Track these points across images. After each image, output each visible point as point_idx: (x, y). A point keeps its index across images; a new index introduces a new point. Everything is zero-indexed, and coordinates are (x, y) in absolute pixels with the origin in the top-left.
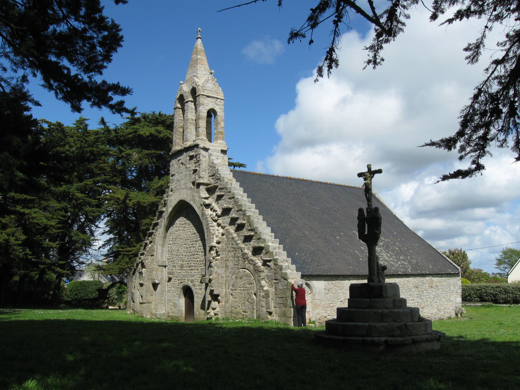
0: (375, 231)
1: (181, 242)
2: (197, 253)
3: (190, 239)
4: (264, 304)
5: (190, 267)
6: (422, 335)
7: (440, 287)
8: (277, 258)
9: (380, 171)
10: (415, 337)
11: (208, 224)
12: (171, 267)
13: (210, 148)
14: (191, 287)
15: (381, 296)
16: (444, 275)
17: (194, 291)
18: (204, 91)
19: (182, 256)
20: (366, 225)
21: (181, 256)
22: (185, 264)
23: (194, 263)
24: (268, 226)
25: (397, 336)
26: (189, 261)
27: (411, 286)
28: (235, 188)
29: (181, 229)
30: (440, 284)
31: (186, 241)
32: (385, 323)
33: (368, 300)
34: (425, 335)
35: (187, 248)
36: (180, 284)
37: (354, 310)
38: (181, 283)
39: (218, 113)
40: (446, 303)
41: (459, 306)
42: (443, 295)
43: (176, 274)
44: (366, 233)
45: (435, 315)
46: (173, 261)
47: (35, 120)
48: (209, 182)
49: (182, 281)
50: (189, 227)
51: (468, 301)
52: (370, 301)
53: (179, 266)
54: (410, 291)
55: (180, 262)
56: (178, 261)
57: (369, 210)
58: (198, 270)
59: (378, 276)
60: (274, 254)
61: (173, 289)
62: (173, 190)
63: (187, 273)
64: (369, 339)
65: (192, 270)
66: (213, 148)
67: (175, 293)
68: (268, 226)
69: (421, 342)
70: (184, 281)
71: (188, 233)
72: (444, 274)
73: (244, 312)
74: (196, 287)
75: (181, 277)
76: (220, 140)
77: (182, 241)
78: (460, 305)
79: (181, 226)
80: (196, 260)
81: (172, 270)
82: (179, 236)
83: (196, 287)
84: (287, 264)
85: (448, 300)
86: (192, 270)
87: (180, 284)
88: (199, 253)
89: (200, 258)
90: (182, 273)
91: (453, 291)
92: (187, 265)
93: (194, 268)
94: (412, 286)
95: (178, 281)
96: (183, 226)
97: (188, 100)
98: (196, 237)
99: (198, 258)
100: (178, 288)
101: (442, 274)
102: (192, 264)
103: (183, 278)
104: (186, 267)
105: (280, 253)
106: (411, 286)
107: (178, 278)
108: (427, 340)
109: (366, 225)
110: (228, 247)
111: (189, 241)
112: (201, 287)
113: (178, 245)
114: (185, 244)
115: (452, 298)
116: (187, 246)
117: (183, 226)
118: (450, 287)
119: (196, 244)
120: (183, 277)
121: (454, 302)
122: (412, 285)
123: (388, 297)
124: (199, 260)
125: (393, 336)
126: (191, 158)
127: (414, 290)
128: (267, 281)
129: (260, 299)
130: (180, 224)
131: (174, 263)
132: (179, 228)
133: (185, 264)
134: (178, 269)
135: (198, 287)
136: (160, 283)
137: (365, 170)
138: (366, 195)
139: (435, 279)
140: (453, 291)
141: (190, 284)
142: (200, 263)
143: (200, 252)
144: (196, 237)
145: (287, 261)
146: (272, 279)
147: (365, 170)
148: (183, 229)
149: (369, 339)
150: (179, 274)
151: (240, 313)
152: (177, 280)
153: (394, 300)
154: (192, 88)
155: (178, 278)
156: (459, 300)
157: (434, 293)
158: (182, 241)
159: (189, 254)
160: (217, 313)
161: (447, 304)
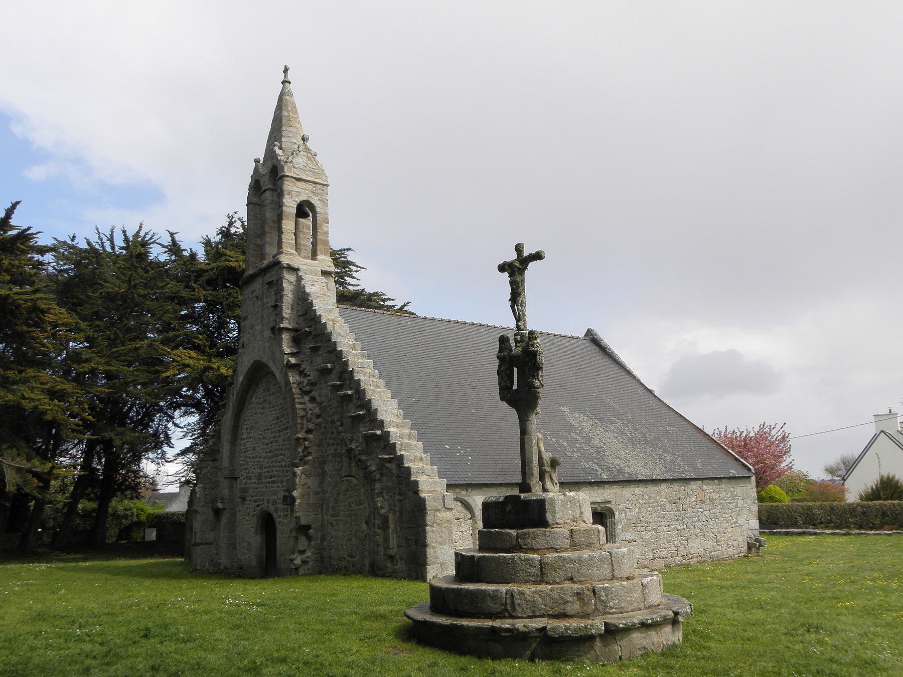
0: (530, 380)
1: (259, 434)
2: (281, 452)
3: (272, 427)
4: (380, 539)
5: (271, 478)
6: (633, 611)
7: (717, 501)
8: (403, 454)
9: (538, 256)
10: (613, 619)
11: (294, 399)
12: (244, 479)
13: (301, 267)
14: (271, 512)
15: (542, 523)
16: (724, 481)
17: (277, 520)
18: (290, 172)
19: (260, 458)
20: (515, 369)
21: (258, 459)
22: (265, 473)
23: (276, 471)
24: (393, 397)
25: (571, 617)
26: (269, 467)
27: (662, 501)
28: (339, 334)
29: (258, 411)
30: (717, 496)
31: (266, 432)
32: (548, 583)
33: (514, 532)
34: (640, 609)
35: (267, 445)
36: (256, 508)
37: (483, 554)
38: (258, 506)
39: (318, 210)
40: (730, 530)
41: (754, 535)
42: (724, 515)
43: (251, 490)
44: (515, 387)
45: (710, 552)
46: (247, 468)
47: (24, 236)
48: (298, 326)
49: (260, 503)
50: (270, 408)
51: (390, 576)
52: (518, 533)
53: (256, 476)
54: (663, 509)
55: (256, 470)
56: (254, 468)
57: (518, 338)
58: (282, 482)
59: (542, 478)
60: (398, 447)
61: (247, 518)
62: (245, 344)
63: (267, 489)
64: (506, 624)
65: (273, 482)
66: (305, 267)
67: (250, 526)
68: (393, 397)
69: (628, 630)
70: (263, 502)
71: (269, 417)
72: (725, 478)
73: (349, 556)
74: (279, 514)
75: (258, 495)
76: (322, 254)
77: (259, 432)
78: (757, 533)
79: (259, 406)
80: (280, 464)
81: (246, 483)
82: (256, 423)
83: (279, 514)
84: (421, 465)
85: (734, 526)
86: (273, 482)
87: (256, 508)
88: (283, 452)
89: (286, 461)
90: (260, 489)
91: (741, 509)
92: (267, 474)
93: (277, 478)
94: (665, 500)
95: (254, 504)
96: (261, 406)
97: (267, 188)
98: (279, 424)
99: (283, 460)
100: (254, 515)
101: (720, 478)
102: (274, 473)
103: (261, 498)
104: (266, 477)
105: (408, 445)
106: (662, 501)
107: (254, 498)
108: (645, 626)
109: (515, 369)
110: (325, 439)
111: (270, 431)
112: (286, 513)
113: (254, 440)
114: (264, 438)
115: (741, 520)
116: (267, 441)
117: (261, 406)
118: (735, 501)
119: (280, 436)
120: (261, 496)
121: (744, 528)
122: (666, 498)
123: (557, 523)
124: (284, 463)
125: (564, 616)
126: (270, 284)
127: (668, 507)
128: (386, 497)
129: (375, 532)
130: (257, 403)
131: (249, 473)
132: (255, 411)
133: (265, 473)
134: (255, 483)
135: (282, 513)
136: (226, 509)
137: (512, 256)
138: (512, 307)
139: (708, 487)
140: (741, 509)
141: (272, 509)
142: (285, 469)
143: (285, 450)
144: (279, 424)
145: (421, 459)
146: (395, 493)
147: (512, 256)
148: (261, 411)
149: (506, 624)
150: (256, 491)
151: (345, 559)
152: (252, 502)
153: (572, 530)
154: (271, 166)
155: (254, 498)
156: (755, 523)
157: (707, 513)
158: (259, 432)
159: (270, 454)
160: (307, 559)
161: (732, 532)
